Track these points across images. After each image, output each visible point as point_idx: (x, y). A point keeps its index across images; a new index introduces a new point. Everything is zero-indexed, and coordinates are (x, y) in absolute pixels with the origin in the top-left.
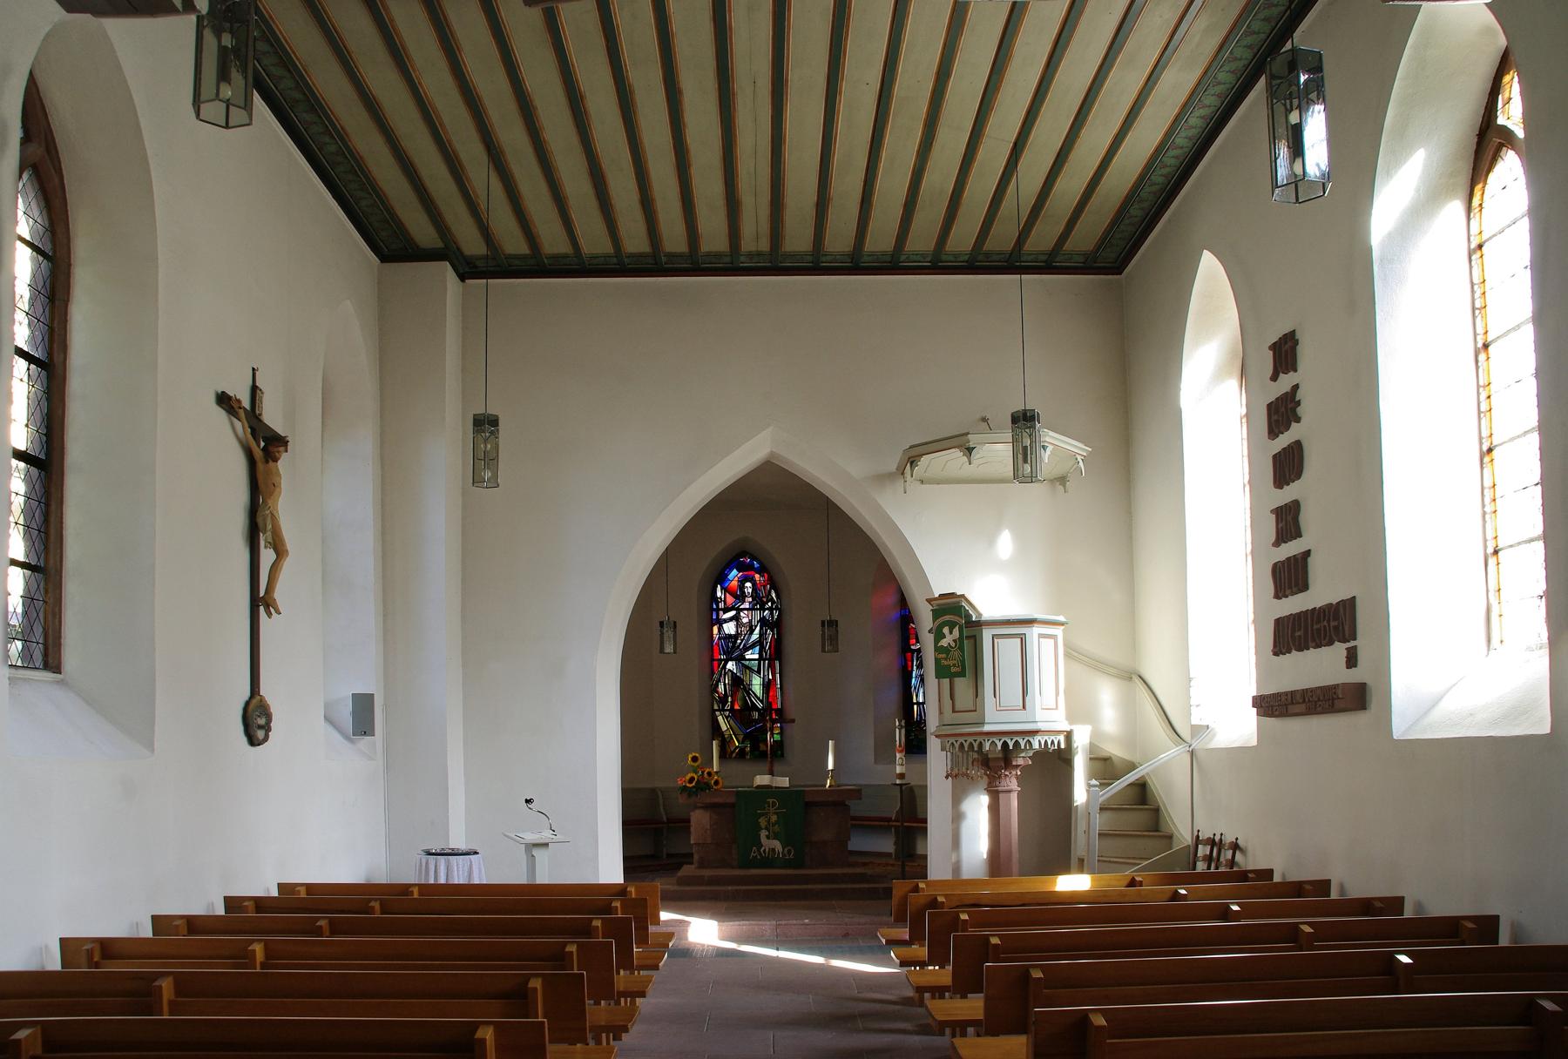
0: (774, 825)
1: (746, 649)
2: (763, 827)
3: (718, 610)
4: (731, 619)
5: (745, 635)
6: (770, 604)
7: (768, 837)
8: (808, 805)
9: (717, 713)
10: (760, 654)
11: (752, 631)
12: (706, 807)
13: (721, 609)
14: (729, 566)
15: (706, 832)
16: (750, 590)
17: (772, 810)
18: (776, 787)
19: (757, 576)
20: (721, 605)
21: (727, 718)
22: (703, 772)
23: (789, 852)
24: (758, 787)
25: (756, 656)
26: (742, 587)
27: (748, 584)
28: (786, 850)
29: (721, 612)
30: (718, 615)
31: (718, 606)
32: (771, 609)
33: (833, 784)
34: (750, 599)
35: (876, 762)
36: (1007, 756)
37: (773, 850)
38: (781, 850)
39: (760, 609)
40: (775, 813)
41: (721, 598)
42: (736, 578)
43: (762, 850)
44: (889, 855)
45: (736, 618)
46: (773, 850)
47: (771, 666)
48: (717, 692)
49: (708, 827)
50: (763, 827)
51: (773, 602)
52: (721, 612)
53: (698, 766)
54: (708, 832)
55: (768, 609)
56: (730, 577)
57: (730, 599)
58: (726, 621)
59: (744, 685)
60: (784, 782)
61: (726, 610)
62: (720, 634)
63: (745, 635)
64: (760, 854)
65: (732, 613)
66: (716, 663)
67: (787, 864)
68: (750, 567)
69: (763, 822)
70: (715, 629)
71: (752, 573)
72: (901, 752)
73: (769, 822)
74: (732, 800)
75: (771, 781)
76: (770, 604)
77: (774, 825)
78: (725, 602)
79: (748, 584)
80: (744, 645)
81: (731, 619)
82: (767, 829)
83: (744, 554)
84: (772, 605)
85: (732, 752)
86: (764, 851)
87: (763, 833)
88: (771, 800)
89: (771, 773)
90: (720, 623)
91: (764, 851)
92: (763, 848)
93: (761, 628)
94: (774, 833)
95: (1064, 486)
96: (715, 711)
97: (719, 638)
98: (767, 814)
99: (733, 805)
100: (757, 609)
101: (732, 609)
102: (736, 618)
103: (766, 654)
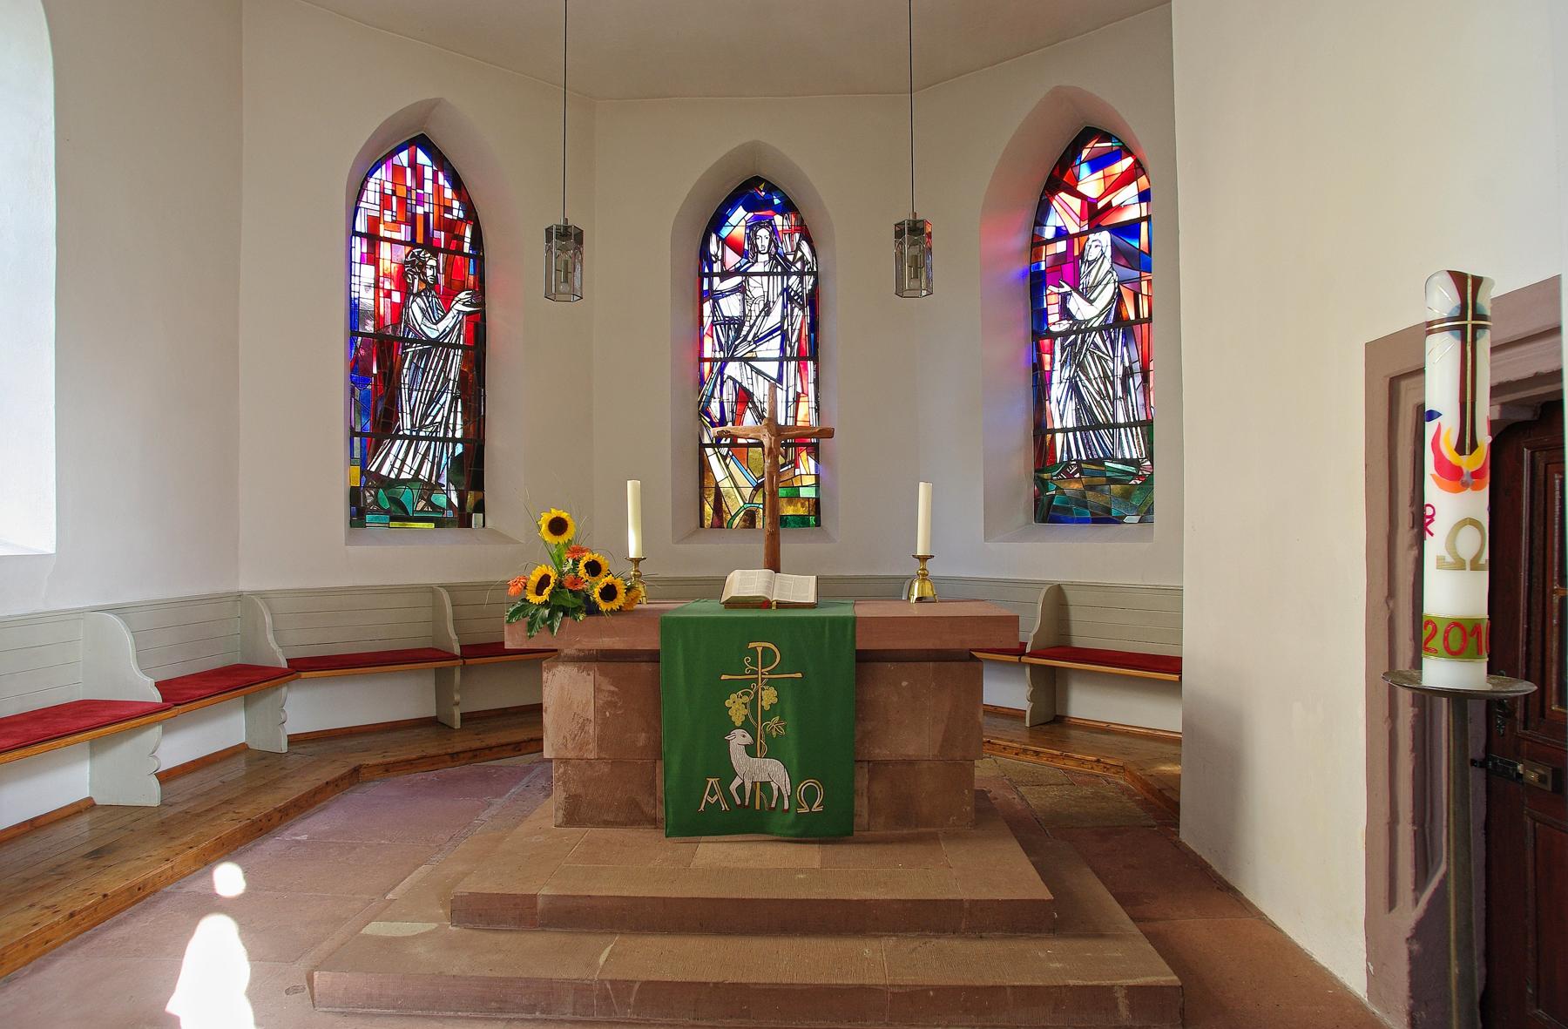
0: (767, 716)
1: (758, 340)
2: (738, 723)
3: (711, 275)
4: (733, 291)
5: (757, 317)
6: (799, 265)
7: (751, 750)
8: (865, 658)
9: (709, 451)
10: (782, 349)
11: (767, 310)
12: (587, 659)
13: (717, 275)
14: (731, 203)
15: (582, 728)
16: (766, 243)
17: (763, 673)
18: (781, 605)
19: (778, 219)
20: (717, 268)
21: (724, 458)
22: (576, 562)
23: (810, 795)
24: (734, 603)
25: (777, 354)
26: (752, 236)
27: (763, 233)
28: (803, 786)
29: (716, 280)
30: (711, 284)
31: (711, 268)
32: (801, 274)
33: (928, 592)
34: (766, 257)
35: (985, 541)
36: (448, 523)
37: (765, 786)
38: (787, 789)
39: (782, 274)
40: (770, 683)
41: (716, 255)
42: (743, 223)
43: (733, 787)
44: (1017, 715)
45: (741, 289)
46: (765, 786)
47: (801, 370)
48: (708, 415)
49: (591, 715)
50: (738, 723)
51: (805, 263)
52: (716, 280)
53: (567, 545)
54: (591, 729)
55: (795, 273)
56: (733, 220)
57: (732, 259)
58: (723, 294)
59: (753, 403)
60: (799, 588)
61: (725, 275)
62: (714, 315)
63: (757, 317)
64: (728, 796)
65: (737, 280)
66: (707, 366)
67: (808, 832)
68: (768, 204)
69: (736, 707)
70: (707, 307)
71: (769, 213)
72: (1452, 475)
73: (753, 705)
74: (648, 641)
75: (770, 586)
76: (799, 265)
77: (767, 716)
78: (723, 264)
79: (763, 233)
80: (754, 337)
81: (733, 291)
82: (747, 726)
83: (757, 180)
84: (803, 266)
85: (733, 517)
86: (741, 788)
87: (738, 740)
88: (759, 646)
89: (774, 564)
90: (714, 296)
91: (741, 788)
92: (737, 782)
93: (784, 306)
94: (768, 737)
95: (1061, 320)
96: (702, 446)
97: (713, 324)
98: (746, 684)
99: (653, 657)
100: (777, 274)
101: (737, 272)
102: (741, 289)
103: (792, 348)
